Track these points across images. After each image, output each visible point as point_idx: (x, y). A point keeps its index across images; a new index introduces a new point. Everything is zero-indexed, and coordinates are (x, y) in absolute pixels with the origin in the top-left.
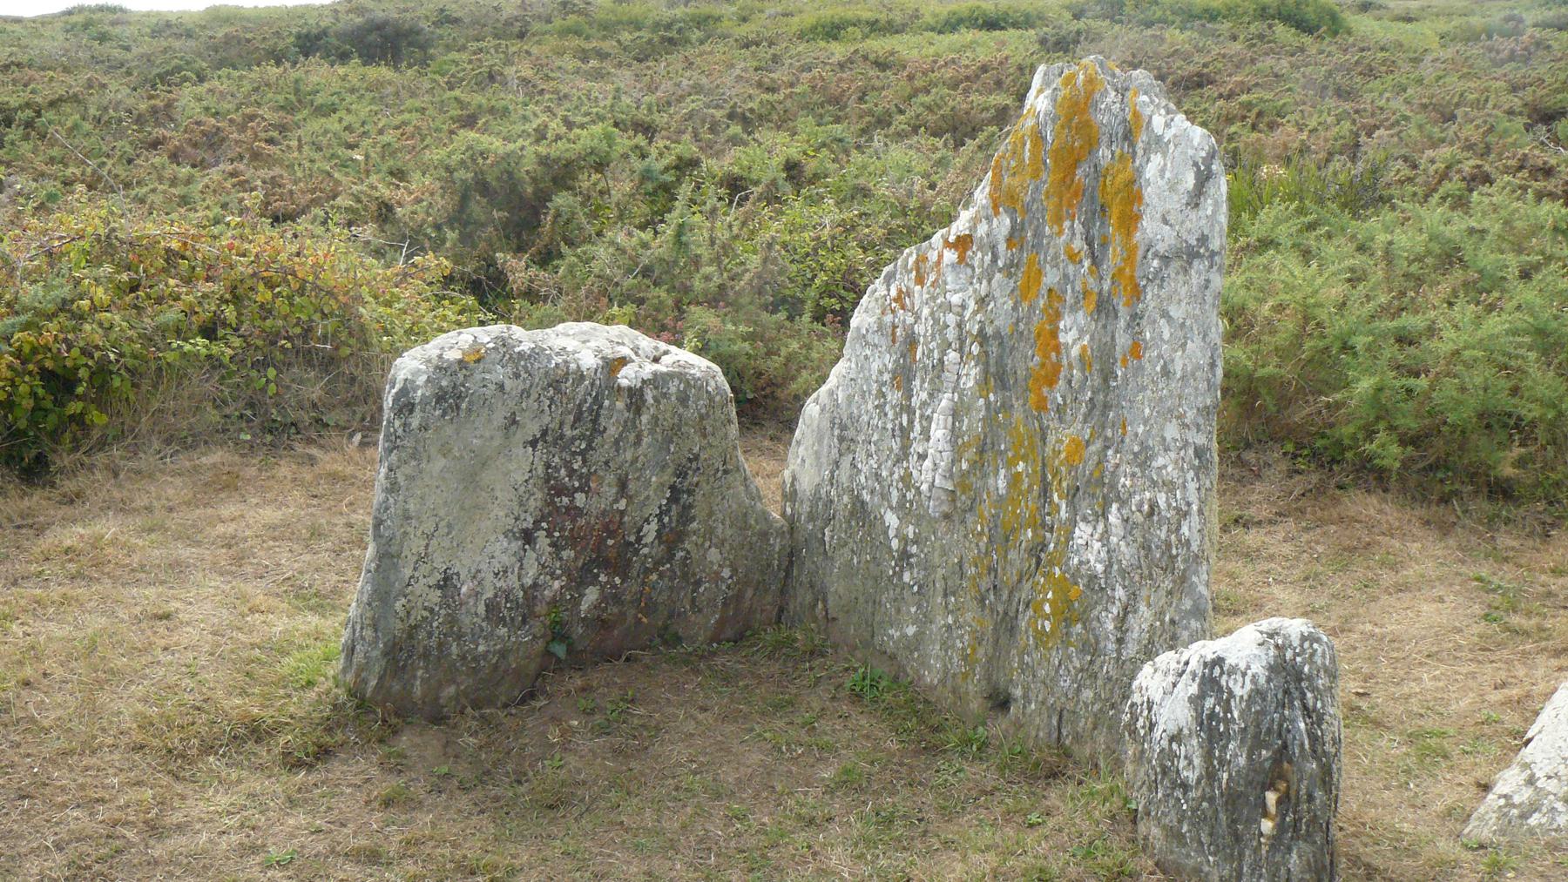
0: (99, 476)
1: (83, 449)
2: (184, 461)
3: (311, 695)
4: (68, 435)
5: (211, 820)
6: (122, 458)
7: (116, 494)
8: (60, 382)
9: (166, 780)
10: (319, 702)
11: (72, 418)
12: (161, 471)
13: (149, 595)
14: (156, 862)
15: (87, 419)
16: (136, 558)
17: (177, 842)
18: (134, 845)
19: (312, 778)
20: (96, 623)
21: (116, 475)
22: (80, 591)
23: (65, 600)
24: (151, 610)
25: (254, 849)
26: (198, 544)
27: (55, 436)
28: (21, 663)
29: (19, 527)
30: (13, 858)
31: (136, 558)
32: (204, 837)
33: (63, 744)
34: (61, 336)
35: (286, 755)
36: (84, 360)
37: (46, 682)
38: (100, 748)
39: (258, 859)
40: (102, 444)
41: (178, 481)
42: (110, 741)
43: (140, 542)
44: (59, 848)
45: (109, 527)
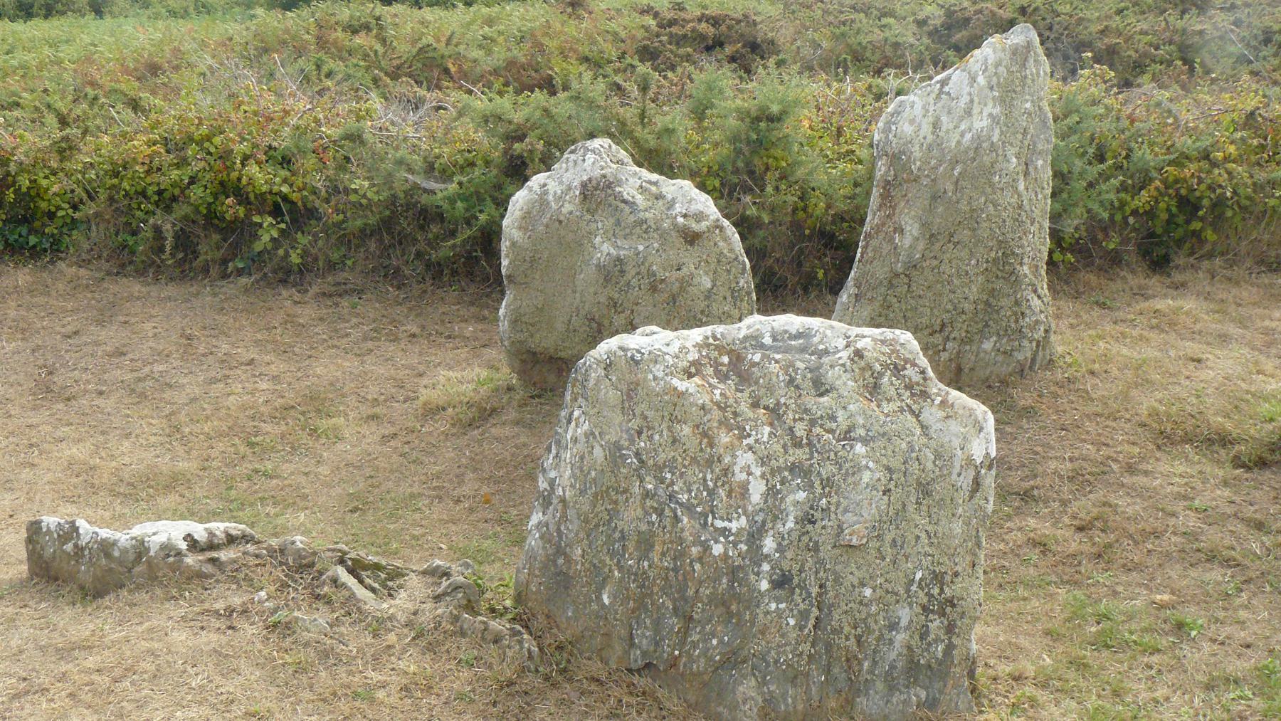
0: (1201, 275)
1: (1196, 256)
2: (1265, 279)
3: (1270, 427)
4: (1188, 245)
5: (1168, 476)
6: (1220, 267)
7: (1208, 289)
8: (1188, 205)
9: (1151, 446)
10: (1273, 432)
11: (1194, 232)
12: (1245, 281)
13: (1192, 348)
14: (1123, 485)
15: (1203, 235)
16: (1198, 327)
17: (1141, 480)
18: (1114, 472)
19: (1246, 475)
20: (1151, 353)
21: (1213, 277)
22: (1153, 335)
23: (1141, 337)
24: (1190, 355)
25: (1185, 498)
26: (1246, 327)
27: (1180, 243)
28: (1094, 362)
29: (1135, 294)
30: (1044, 458)
31: (1198, 327)
32: (1158, 482)
33: (1099, 410)
34: (1197, 174)
35: (1236, 457)
36: (1208, 193)
37: (1105, 375)
38: (1120, 418)
39: (1185, 503)
40: (1210, 255)
41: (1255, 290)
42: (1128, 416)
43: (1206, 317)
44: (1071, 460)
45: (1189, 304)
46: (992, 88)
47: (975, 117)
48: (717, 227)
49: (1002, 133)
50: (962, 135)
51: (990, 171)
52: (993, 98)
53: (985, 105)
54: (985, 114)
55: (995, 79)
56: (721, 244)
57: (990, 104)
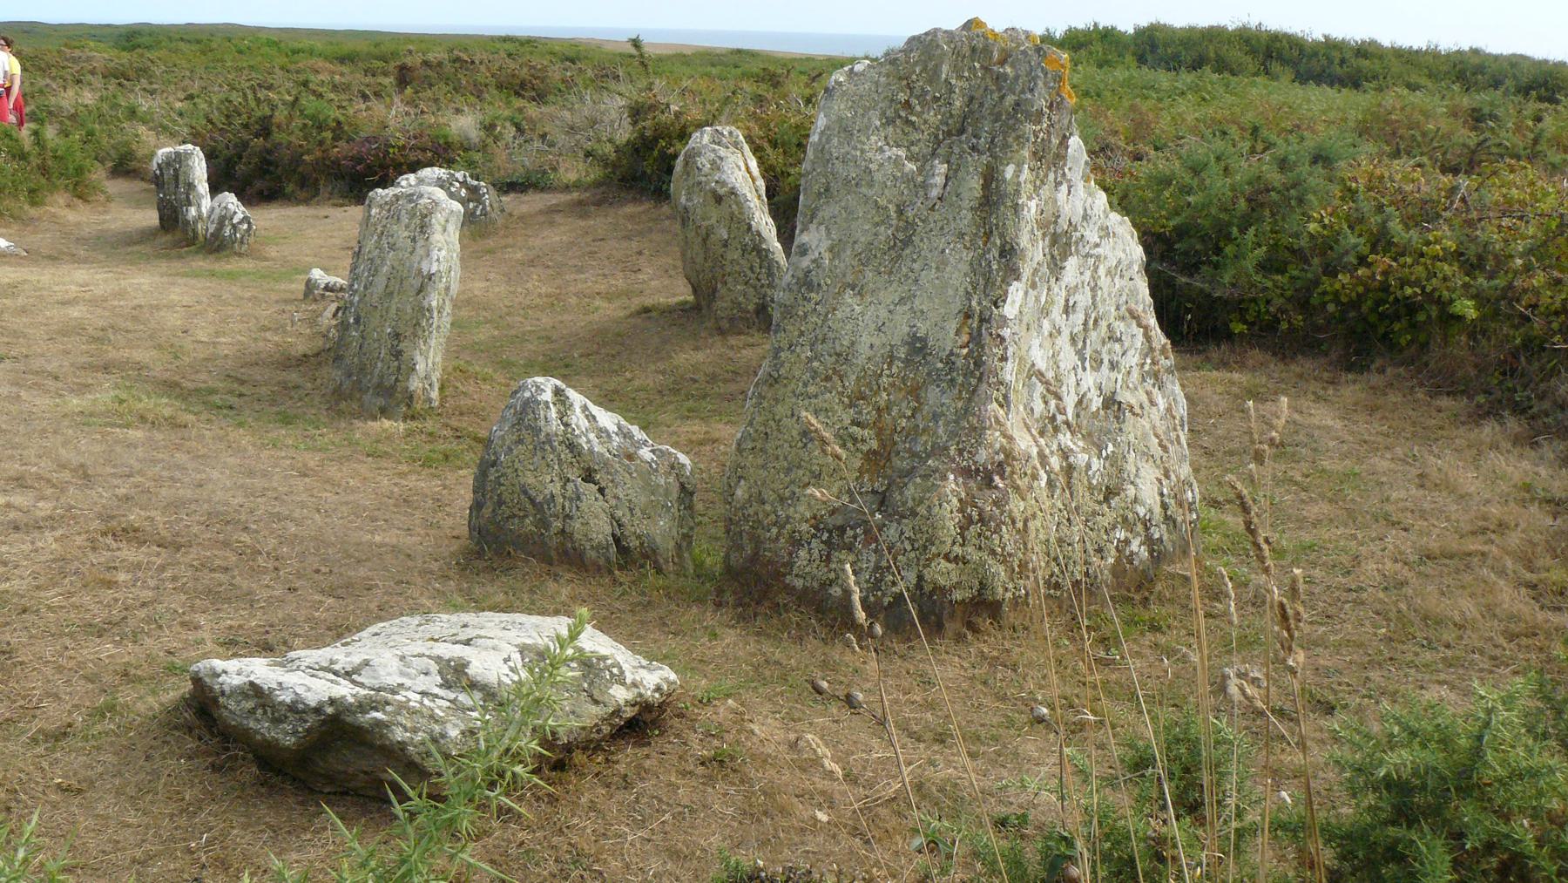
56: (734, 206)
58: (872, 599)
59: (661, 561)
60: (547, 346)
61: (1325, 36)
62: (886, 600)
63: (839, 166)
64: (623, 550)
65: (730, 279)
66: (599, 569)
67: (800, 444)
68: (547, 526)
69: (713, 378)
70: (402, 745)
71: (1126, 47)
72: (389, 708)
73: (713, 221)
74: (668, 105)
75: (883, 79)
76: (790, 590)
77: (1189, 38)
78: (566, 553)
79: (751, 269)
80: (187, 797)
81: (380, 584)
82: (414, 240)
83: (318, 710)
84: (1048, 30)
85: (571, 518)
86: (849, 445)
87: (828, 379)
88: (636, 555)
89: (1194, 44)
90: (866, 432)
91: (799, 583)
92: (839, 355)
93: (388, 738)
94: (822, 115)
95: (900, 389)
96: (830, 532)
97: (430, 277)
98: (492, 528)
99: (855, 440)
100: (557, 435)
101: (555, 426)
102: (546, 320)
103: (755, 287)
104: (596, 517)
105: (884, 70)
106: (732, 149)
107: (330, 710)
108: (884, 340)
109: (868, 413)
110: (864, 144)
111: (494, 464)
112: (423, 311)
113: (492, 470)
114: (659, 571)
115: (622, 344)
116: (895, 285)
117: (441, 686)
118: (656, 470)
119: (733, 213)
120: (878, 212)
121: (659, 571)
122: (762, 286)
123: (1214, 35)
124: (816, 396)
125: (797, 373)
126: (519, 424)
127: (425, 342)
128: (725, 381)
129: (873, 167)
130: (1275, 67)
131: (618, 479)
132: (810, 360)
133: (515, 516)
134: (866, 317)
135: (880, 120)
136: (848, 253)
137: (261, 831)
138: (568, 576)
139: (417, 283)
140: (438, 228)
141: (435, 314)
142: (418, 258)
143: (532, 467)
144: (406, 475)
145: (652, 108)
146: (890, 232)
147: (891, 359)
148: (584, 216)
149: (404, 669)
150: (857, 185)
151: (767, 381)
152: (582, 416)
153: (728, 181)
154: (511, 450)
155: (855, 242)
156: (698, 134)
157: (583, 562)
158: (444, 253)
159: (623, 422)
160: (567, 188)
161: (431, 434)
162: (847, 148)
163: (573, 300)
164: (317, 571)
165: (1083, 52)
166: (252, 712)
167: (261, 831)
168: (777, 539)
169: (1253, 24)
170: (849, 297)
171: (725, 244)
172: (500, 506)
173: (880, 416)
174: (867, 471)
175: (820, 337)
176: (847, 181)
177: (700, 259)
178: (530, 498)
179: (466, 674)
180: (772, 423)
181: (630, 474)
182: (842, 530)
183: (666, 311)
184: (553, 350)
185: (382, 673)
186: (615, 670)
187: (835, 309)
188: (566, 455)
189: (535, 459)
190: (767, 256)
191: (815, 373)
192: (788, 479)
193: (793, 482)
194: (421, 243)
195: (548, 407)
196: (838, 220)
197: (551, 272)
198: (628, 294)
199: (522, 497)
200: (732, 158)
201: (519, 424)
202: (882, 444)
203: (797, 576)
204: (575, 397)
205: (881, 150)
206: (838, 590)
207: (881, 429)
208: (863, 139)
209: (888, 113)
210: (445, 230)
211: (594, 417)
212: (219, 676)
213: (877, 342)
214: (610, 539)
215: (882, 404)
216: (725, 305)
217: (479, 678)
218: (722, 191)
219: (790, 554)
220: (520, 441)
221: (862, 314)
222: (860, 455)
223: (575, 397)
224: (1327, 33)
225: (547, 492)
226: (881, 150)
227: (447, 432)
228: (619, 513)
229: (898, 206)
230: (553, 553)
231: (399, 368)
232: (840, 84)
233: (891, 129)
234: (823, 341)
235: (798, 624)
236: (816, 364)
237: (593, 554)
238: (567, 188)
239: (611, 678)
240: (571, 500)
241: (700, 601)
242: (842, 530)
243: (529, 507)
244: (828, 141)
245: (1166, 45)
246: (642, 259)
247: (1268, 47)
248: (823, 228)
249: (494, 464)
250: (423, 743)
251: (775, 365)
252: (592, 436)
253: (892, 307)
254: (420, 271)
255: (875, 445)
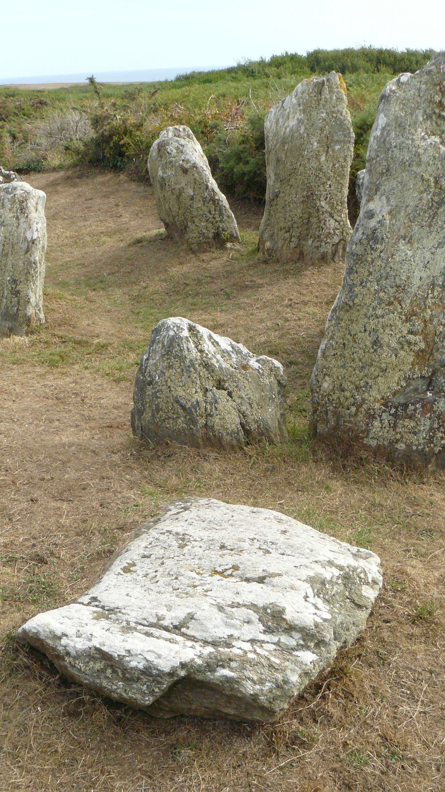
46: (299, 105)
47: (290, 120)
48: (194, 167)
49: (306, 129)
50: (286, 129)
51: (300, 148)
52: (300, 110)
53: (296, 114)
54: (295, 118)
55: (301, 100)
56: (196, 175)
57: (298, 114)
58: (427, 449)
59: (273, 436)
60: (84, 270)
61: (407, 49)
62: (437, 450)
63: (396, 151)
64: (247, 432)
65: (196, 220)
66: (233, 447)
67: (372, 350)
68: (195, 423)
69: (199, 282)
70: (255, 697)
71: (304, 63)
72: (233, 664)
73: (183, 185)
74: (115, 116)
75: (423, 87)
76: (367, 448)
77: (336, 56)
78: (209, 439)
79: (210, 212)
80: (60, 750)
81: (90, 483)
82: (17, 218)
83: (171, 674)
84: (262, 58)
85: (211, 416)
86: (406, 347)
87: (390, 304)
88: (255, 434)
89: (339, 59)
90: (417, 337)
91: (374, 443)
92: (398, 287)
93: (241, 692)
94: (382, 115)
95: (439, 306)
96: (396, 408)
97: (33, 242)
98: (152, 427)
99: (409, 343)
100: (196, 359)
101: (195, 353)
102: (77, 253)
103: (212, 223)
104: (229, 413)
105: (423, 80)
106: (187, 139)
107: (183, 673)
108: (429, 273)
109: (419, 325)
110: (413, 135)
111: (150, 383)
112: (31, 264)
113: (149, 388)
114: (271, 442)
115: (133, 265)
116: (434, 234)
117: (265, 632)
118: (263, 374)
119: (195, 179)
120: (423, 183)
121: (271, 442)
122: (216, 222)
123: (348, 53)
124: (383, 317)
125: (368, 302)
126: (167, 354)
127: (34, 283)
128: (207, 283)
129: (421, 151)
130: (382, 68)
131: (241, 384)
132: (377, 292)
133: (169, 418)
134: (417, 258)
135: (423, 116)
136: (402, 214)
137: (138, 779)
138: (213, 455)
139: (24, 246)
140: (32, 209)
141: (38, 265)
142: (23, 231)
143: (181, 384)
144: (44, 375)
145: (106, 118)
146: (429, 197)
147: (433, 285)
148: (75, 185)
149: (228, 621)
150: (410, 165)
151: (343, 308)
152: (210, 343)
153: (191, 159)
154: (164, 373)
155: (407, 206)
156: (165, 132)
157: (221, 443)
158: (40, 225)
159: (234, 343)
160: (54, 169)
161: (46, 342)
162: (402, 139)
163: (88, 239)
164: (43, 479)
165: (282, 68)
166: (103, 671)
167: (138, 779)
168: (356, 415)
169: (367, 46)
170: (402, 245)
171: (192, 198)
172: (158, 412)
173: (426, 326)
174: (417, 364)
175: (384, 275)
176: (403, 163)
177: (175, 209)
178: (181, 406)
179: (284, 620)
180: (348, 336)
181: (248, 380)
182: (405, 406)
183: (152, 241)
184: (88, 272)
185: (210, 626)
186: (362, 575)
187: (393, 255)
188: (204, 372)
189: (183, 378)
190: (218, 203)
191: (381, 300)
192: (362, 374)
193: (366, 376)
194: (22, 220)
195: (188, 341)
196: (395, 191)
197: (66, 222)
198: (119, 231)
199: (175, 405)
200: (190, 145)
201: (167, 354)
202: (428, 345)
203: (372, 438)
204: (204, 331)
205: (423, 138)
206: (403, 446)
207: (426, 335)
208: (413, 131)
209: (428, 111)
210: (36, 210)
211: (217, 343)
212: (60, 638)
213: (424, 275)
214: (239, 426)
215: (428, 317)
216: (195, 235)
217: (297, 622)
218: (187, 166)
219: (368, 425)
220: (170, 367)
221: (414, 256)
222: (413, 353)
223: (204, 331)
224: (407, 47)
225: (194, 400)
226: (423, 138)
227: (56, 340)
228: (244, 408)
229: (435, 178)
230: (200, 440)
231: (19, 302)
232: (394, 92)
233: (429, 122)
234: (386, 278)
235: (378, 471)
236: (382, 294)
237: (229, 438)
238: (54, 169)
239: (360, 581)
240: (211, 404)
241: (305, 461)
242: (405, 406)
243: (181, 411)
244: (388, 134)
245: (325, 61)
246: (121, 210)
247: (378, 58)
248: (384, 198)
249: (150, 383)
250: (271, 691)
251: (351, 297)
252: (219, 357)
253: (433, 250)
254: (25, 238)
255: (423, 345)
